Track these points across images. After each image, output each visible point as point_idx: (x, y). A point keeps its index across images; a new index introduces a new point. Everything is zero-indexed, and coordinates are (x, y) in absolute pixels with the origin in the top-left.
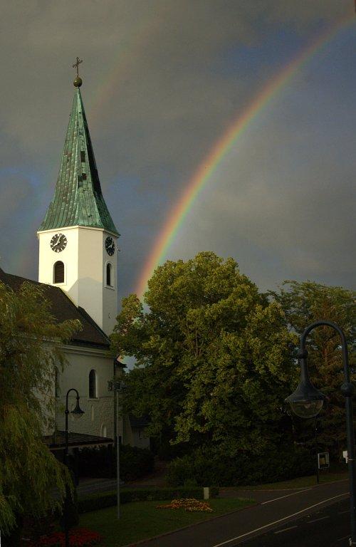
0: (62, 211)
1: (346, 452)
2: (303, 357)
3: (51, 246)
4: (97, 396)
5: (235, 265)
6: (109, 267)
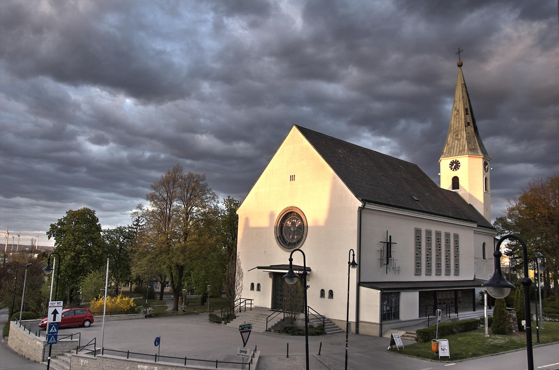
0: (456, 145)
1: (525, 321)
2: (30, 252)
6: (486, 179)
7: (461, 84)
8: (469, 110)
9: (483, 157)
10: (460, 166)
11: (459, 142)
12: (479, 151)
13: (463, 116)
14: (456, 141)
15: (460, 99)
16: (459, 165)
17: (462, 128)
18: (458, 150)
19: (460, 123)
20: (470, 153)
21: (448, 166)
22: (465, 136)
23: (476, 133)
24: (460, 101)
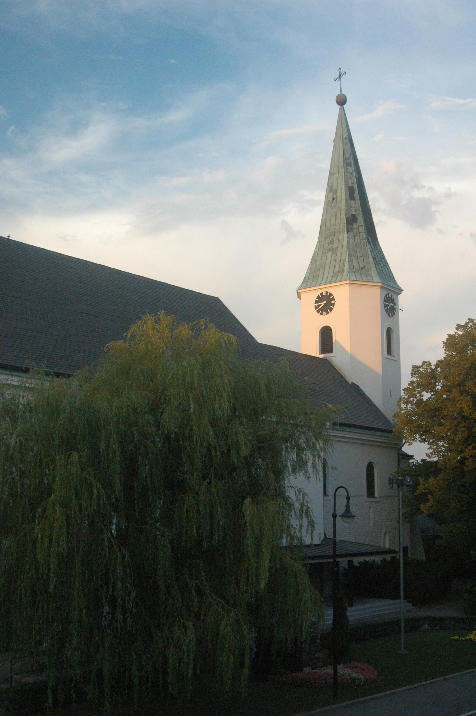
3: (316, 308)
4: (376, 495)
5: (443, 342)
7: (342, 139)
8: (356, 191)
9: (380, 285)
10: (334, 303)
11: (333, 256)
12: (374, 273)
13: (344, 202)
14: (328, 253)
15: (340, 168)
16: (333, 302)
17: (341, 228)
18: (332, 270)
19: (338, 216)
20: (353, 277)
21: (313, 305)
22: (345, 243)
23: (370, 238)
24: (338, 172)
